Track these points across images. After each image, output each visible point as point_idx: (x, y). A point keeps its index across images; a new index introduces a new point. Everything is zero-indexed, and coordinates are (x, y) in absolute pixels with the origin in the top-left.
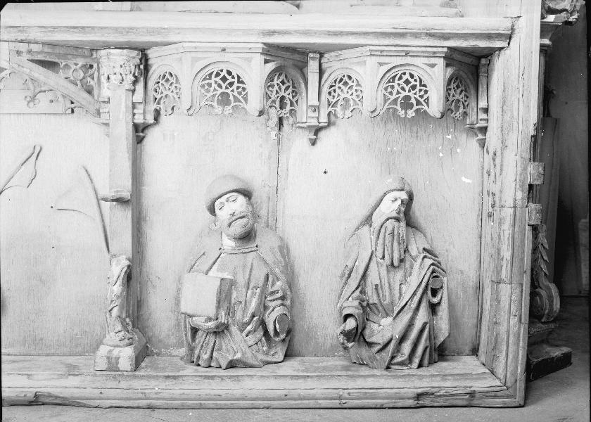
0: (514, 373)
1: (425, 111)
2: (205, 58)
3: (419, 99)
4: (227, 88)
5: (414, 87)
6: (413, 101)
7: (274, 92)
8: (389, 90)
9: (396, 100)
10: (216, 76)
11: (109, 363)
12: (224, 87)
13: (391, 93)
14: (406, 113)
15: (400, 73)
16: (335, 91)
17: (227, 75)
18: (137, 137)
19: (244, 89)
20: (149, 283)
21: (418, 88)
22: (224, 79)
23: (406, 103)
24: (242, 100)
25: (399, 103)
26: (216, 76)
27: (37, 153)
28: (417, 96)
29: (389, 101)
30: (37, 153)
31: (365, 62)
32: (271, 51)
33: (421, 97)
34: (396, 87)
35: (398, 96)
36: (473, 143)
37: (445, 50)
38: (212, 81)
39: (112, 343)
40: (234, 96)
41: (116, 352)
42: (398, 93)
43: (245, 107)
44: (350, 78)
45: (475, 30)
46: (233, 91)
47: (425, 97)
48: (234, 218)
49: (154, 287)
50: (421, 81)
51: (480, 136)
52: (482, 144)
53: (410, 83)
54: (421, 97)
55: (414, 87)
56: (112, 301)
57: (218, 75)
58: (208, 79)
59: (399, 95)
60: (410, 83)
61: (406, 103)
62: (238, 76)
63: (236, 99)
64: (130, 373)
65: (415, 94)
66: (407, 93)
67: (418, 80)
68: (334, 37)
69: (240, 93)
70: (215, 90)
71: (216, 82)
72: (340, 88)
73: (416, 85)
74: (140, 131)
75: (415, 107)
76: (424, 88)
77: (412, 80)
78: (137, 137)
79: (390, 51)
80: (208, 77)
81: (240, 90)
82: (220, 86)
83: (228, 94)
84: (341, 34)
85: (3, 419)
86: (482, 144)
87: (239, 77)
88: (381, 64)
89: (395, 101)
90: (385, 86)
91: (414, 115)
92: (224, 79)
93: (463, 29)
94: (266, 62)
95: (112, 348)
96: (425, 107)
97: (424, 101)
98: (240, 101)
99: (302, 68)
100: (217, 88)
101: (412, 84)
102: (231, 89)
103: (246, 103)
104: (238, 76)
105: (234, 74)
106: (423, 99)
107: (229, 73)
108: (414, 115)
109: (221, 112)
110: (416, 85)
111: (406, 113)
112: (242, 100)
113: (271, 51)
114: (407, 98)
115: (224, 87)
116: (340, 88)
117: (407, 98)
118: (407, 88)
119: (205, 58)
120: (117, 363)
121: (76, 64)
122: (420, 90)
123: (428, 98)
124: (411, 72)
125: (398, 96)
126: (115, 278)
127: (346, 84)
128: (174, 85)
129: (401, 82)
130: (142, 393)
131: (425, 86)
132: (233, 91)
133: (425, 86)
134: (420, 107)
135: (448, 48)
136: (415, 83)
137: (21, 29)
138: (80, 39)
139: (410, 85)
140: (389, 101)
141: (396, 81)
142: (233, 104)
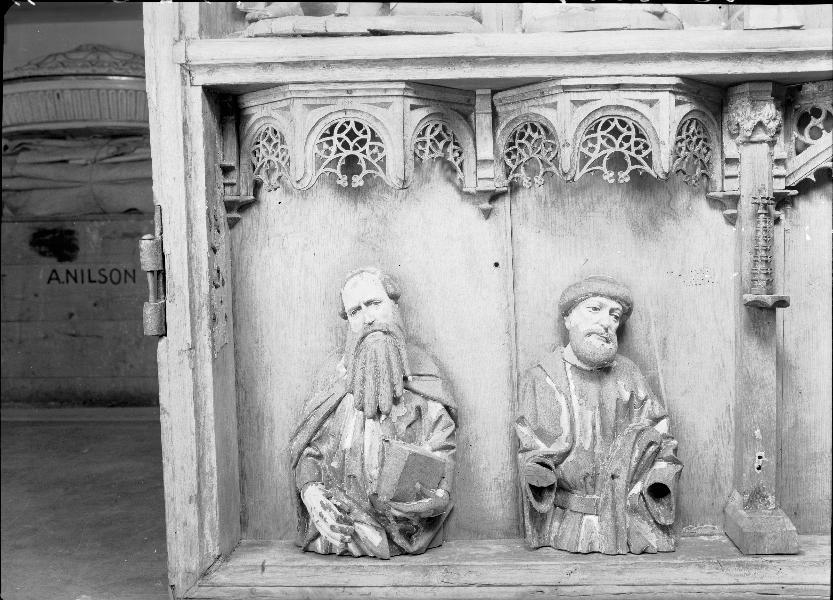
1: (646, 174)
2: (586, 102)
3: (370, 159)
4: (355, 148)
7: (427, 151)
8: (326, 146)
10: (603, 129)
13: (328, 152)
14: (350, 181)
16: (515, 150)
17: (619, 127)
22: (351, 135)
23: (617, 162)
24: (642, 161)
25: (339, 166)
26: (603, 129)
28: (633, 154)
31: (555, 104)
32: (424, 92)
34: (336, 142)
35: (338, 156)
36: (716, 217)
38: (600, 133)
40: (632, 158)
42: (603, 148)
43: (382, 175)
47: (380, 156)
48: (372, 328)
50: (637, 130)
53: (621, 133)
55: (627, 139)
58: (328, 136)
59: (340, 154)
60: (621, 133)
61: (617, 162)
62: (371, 130)
66: (617, 149)
67: (633, 130)
70: (338, 151)
71: (340, 139)
75: (631, 168)
76: (379, 144)
77: (359, 133)
80: (328, 132)
84: (542, 60)
89: (599, 161)
90: (585, 138)
92: (351, 135)
94: (678, 103)
96: (646, 168)
97: (378, 162)
98: (641, 164)
99: (467, 117)
100: (341, 149)
101: (358, 139)
102: (361, 149)
103: (384, 171)
104: (371, 130)
105: (630, 123)
106: (376, 160)
107: (359, 126)
109: (346, 184)
111: (350, 181)
112: (642, 161)
113: (424, 92)
114: (352, 159)
115: (617, 145)
116: (521, 145)
117: (352, 159)
122: (371, 147)
123: (650, 154)
124: (357, 120)
125: (338, 156)
128: (280, 147)
129: (343, 135)
132: (364, 152)
134: (372, 172)
136: (628, 133)
137: (61, 59)
138: (759, 71)
140: (589, 163)
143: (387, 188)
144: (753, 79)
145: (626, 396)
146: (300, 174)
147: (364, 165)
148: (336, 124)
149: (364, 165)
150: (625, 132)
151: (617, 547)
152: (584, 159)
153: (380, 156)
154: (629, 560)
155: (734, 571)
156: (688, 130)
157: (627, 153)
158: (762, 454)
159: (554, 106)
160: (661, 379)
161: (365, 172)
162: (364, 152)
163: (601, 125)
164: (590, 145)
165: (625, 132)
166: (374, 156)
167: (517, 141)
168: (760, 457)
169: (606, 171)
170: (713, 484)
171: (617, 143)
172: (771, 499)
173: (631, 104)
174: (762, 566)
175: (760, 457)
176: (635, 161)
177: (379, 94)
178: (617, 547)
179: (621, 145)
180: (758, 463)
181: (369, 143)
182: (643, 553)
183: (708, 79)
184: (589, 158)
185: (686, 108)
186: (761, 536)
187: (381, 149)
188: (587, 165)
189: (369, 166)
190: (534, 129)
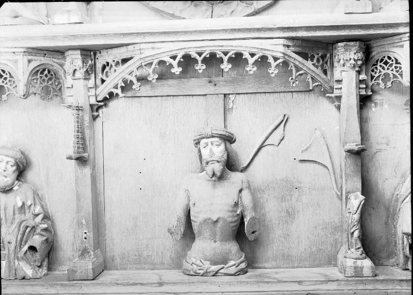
4: (388, 69)
6: (391, 76)
9: (379, 76)
10: (381, 62)
11: (355, 272)
12: (386, 69)
18: (93, 116)
20: (366, 212)
24: (399, 76)
27: (285, 121)
30: (285, 121)
39: (355, 257)
41: (359, 263)
44: (389, 58)
47: (400, 71)
49: (370, 215)
51: (337, 103)
52: (339, 108)
55: (5, 79)
56: (354, 226)
57: (382, 60)
62: (395, 58)
63: (395, 76)
64: (372, 278)
66: (386, 71)
67: (394, 61)
68: (271, 32)
70: (380, 72)
73: (7, 78)
74: (364, 101)
78: (93, 116)
82: (383, 68)
83: (389, 74)
85: (3, 293)
86: (339, 108)
87: (396, 60)
93: (323, 23)
95: (356, 260)
105: (393, 58)
110: (7, 78)
115: (386, 69)
120: (362, 271)
121: (318, 54)
126: (356, 208)
127: (386, 63)
130: (385, 292)
131: (399, 63)
133: (399, 63)
138: (358, 33)
142: (7, 93)
143: (62, 101)
144: (73, 48)
145: (20, 204)
147: (391, 76)
151: (9, 277)
153: (400, 71)
154: (17, 282)
155: (59, 288)
157: (5, 86)
158: (87, 232)
160: (46, 196)
165: (390, 62)
167: (379, 64)
168: (86, 233)
170: (73, 245)
172: (92, 253)
174: (73, 286)
175: (86, 233)
178: (9, 277)
179: (388, 69)
180: (85, 235)
181: (394, 65)
182: (24, 278)
183: (314, 39)
184: (375, 76)
186: (75, 272)
187: (400, 68)
188: (373, 80)
190: (49, 72)
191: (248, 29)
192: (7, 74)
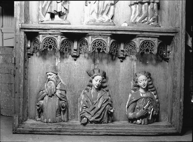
0: (174, 83)
2: (46, 36)
5: (101, 45)
10: (48, 41)
15: (97, 41)
19: (56, 44)
21: (151, 46)
24: (104, 49)
26: (48, 41)
29: (45, 47)
33: (152, 49)
34: (96, 45)
37: (159, 36)
38: (47, 42)
40: (150, 50)
45: (97, 29)
46: (53, 44)
54: (54, 45)
55: (52, 43)
65: (102, 47)
67: (103, 43)
69: (103, 48)
70: (48, 44)
71: (97, 44)
72: (129, 47)
79: (47, 33)
81: (152, 48)
87: (54, 41)
88: (141, 40)
90: (93, 45)
91: (149, 54)
108: (149, 54)
112: (104, 49)
118: (148, 47)
119: (46, 36)
122: (151, 47)
123: (56, 45)
129: (49, 41)
135: (160, 36)
136: (150, 45)
139: (51, 42)
140: (45, 47)
141: (97, 44)
146: (41, 48)
147: (53, 47)
148: (96, 42)
149: (53, 47)
150: (52, 41)
152: (44, 46)
153: (153, 49)
156: (65, 43)
159: (136, 40)
161: (53, 48)
162: (102, 47)
163: (97, 42)
164: (95, 46)
166: (152, 49)
169: (145, 52)
171: (99, 46)
173: (52, 37)
176: (103, 49)
177: (105, 36)
179: (148, 47)
185: (112, 41)
189: (151, 50)
191: (54, 29)
192: (102, 43)
